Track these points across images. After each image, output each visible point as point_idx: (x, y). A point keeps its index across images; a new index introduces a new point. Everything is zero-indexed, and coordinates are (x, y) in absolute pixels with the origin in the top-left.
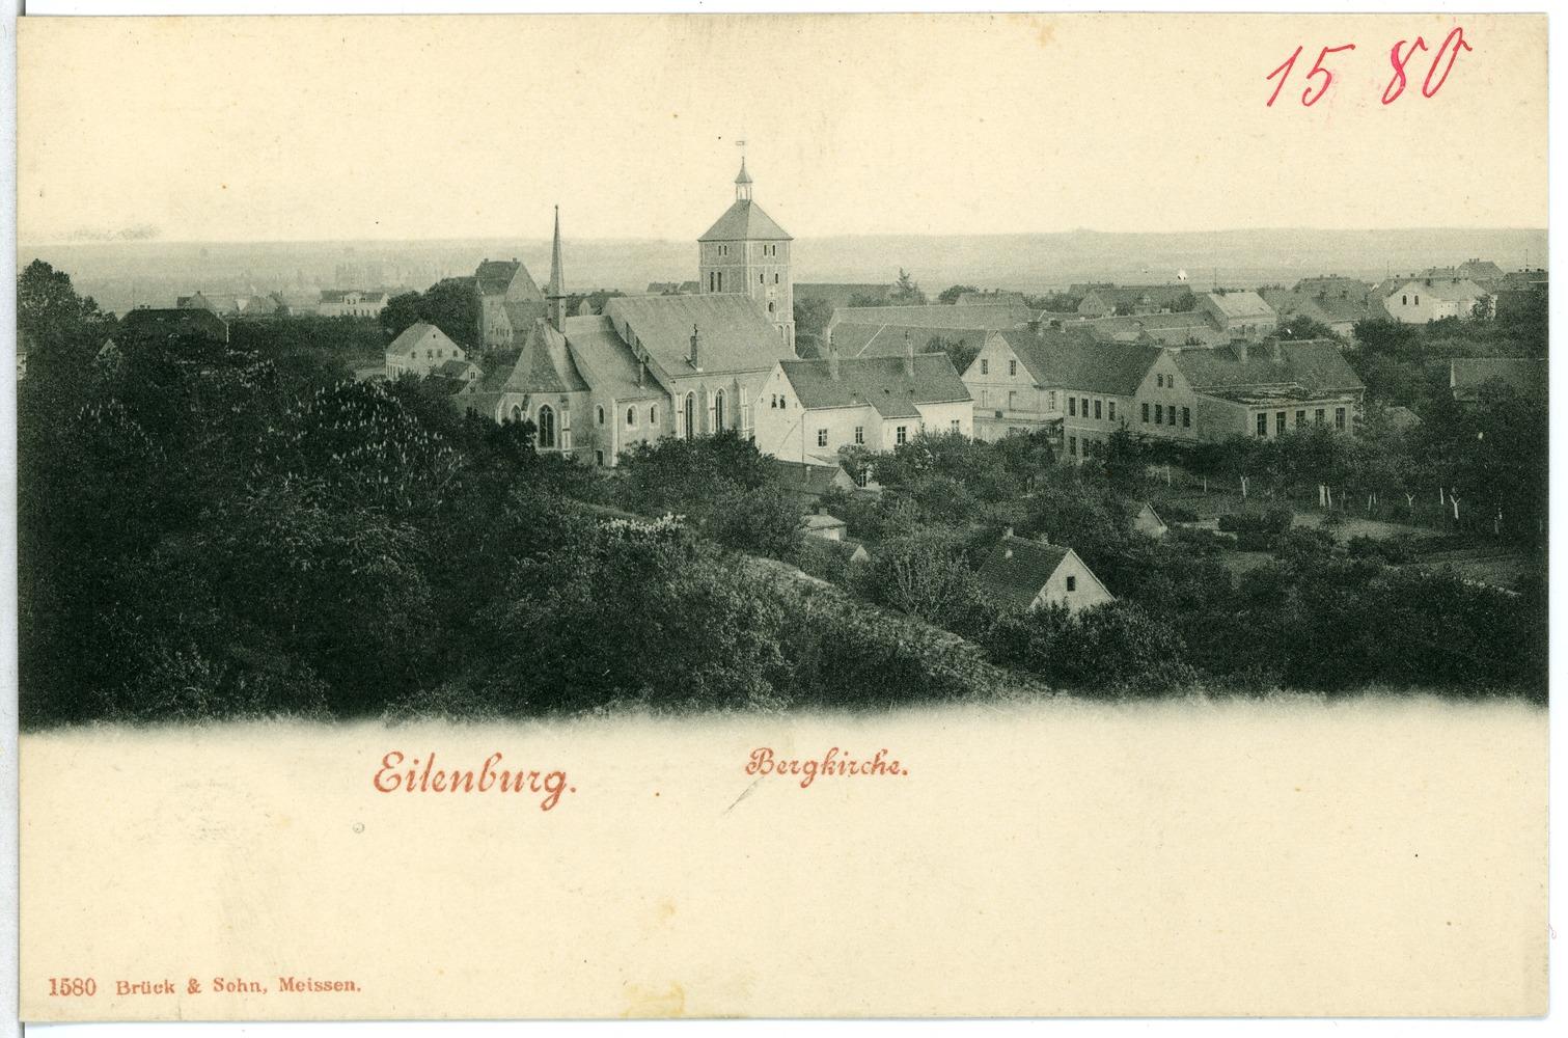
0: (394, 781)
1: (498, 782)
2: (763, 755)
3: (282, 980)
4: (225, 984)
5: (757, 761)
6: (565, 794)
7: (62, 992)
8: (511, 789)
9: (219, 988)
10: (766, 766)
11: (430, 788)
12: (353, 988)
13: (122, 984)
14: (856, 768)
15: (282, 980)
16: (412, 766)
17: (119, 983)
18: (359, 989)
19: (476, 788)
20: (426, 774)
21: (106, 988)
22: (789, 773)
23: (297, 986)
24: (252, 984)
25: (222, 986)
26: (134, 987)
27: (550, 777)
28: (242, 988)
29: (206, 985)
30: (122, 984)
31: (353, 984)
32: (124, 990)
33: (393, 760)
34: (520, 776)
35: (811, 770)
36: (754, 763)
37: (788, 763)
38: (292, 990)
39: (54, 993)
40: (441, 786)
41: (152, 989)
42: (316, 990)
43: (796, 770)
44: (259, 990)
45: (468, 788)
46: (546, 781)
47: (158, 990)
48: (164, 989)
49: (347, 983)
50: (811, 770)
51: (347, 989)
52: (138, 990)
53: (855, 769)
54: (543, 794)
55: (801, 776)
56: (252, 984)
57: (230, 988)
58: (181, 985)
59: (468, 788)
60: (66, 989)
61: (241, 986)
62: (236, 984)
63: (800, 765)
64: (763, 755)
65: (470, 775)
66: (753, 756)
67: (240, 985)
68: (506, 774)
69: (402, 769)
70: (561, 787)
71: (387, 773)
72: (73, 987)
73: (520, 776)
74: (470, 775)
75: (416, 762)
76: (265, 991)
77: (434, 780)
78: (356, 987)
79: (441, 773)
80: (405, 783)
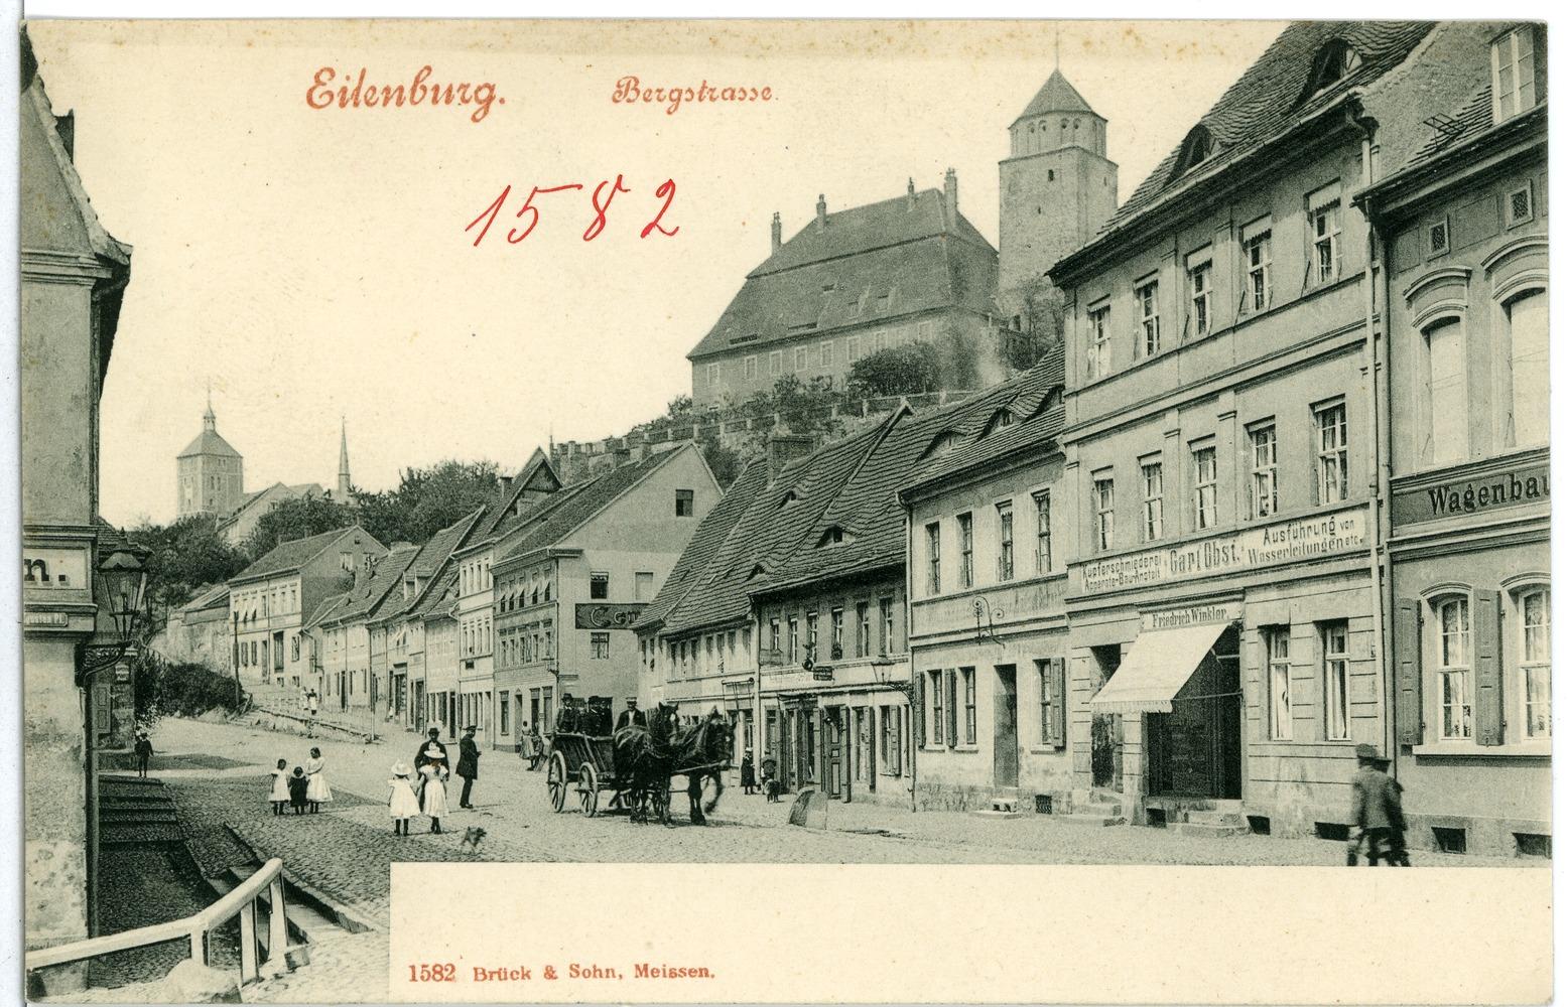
0: (326, 98)
1: (430, 94)
2: (628, 84)
3: (637, 967)
4: (581, 970)
5: (623, 89)
6: (494, 106)
7: (422, 977)
8: (442, 102)
9: (574, 974)
10: (632, 94)
11: (362, 104)
12: (707, 975)
13: (480, 971)
14: (715, 95)
15: (637, 967)
16: (345, 83)
17: (476, 969)
18: (713, 976)
19: (407, 102)
20: (358, 89)
21: (464, 971)
22: (655, 101)
23: (652, 971)
24: (607, 970)
25: (577, 972)
26: (492, 973)
27: (480, 88)
28: (598, 973)
29: (562, 971)
30: (480, 971)
31: (613, 971)
32: (481, 977)
33: (325, 77)
34: (450, 90)
35: (676, 98)
36: (620, 92)
37: (654, 90)
38: (647, 976)
39: (414, 979)
40: (372, 101)
41: (508, 975)
42: (671, 976)
43: (662, 97)
44: (707, 975)
45: (399, 103)
46: (476, 92)
47: (515, 976)
48: (520, 976)
49: (701, 970)
50: (676, 98)
51: (701, 976)
52: (496, 976)
53: (715, 95)
54: (473, 106)
55: (667, 103)
56: (607, 970)
57: (587, 974)
58: (538, 972)
59: (399, 103)
60: (426, 975)
61: (595, 972)
62: (592, 970)
63: (666, 93)
64: (628, 84)
65: (401, 89)
66: (619, 86)
67: (595, 971)
68: (436, 88)
69: (335, 86)
70: (490, 99)
71: (319, 90)
72: (432, 973)
73: (450, 90)
74: (401, 89)
75: (348, 78)
76: (713, 976)
77: (366, 96)
78: (710, 973)
79: (373, 89)
80: (337, 99)
